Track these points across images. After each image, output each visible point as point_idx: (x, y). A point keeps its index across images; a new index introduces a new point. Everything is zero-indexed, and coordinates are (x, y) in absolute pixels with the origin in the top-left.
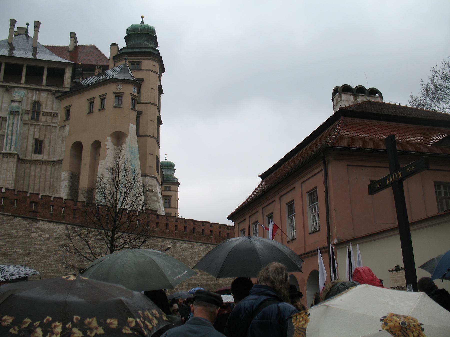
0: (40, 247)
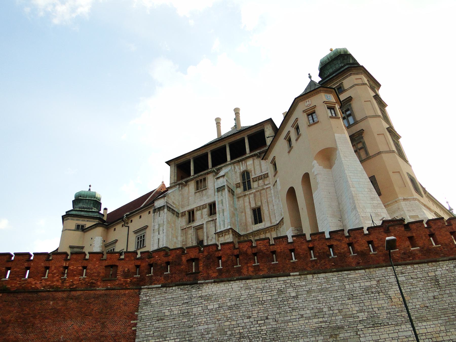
0: (206, 327)
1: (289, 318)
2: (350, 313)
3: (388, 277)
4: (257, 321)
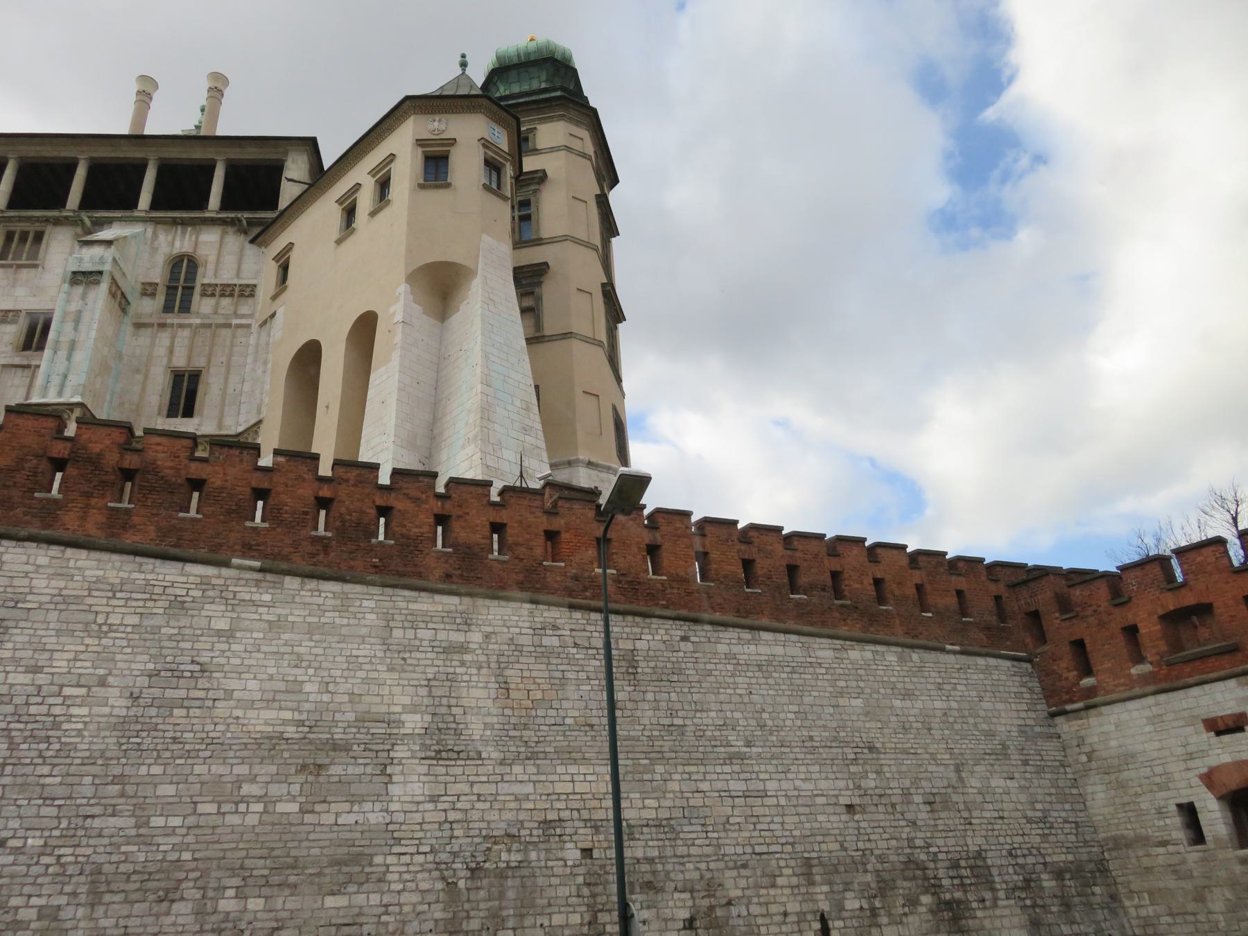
1: (182, 693)
2: (384, 709)
3: (517, 630)
4: (62, 686)
